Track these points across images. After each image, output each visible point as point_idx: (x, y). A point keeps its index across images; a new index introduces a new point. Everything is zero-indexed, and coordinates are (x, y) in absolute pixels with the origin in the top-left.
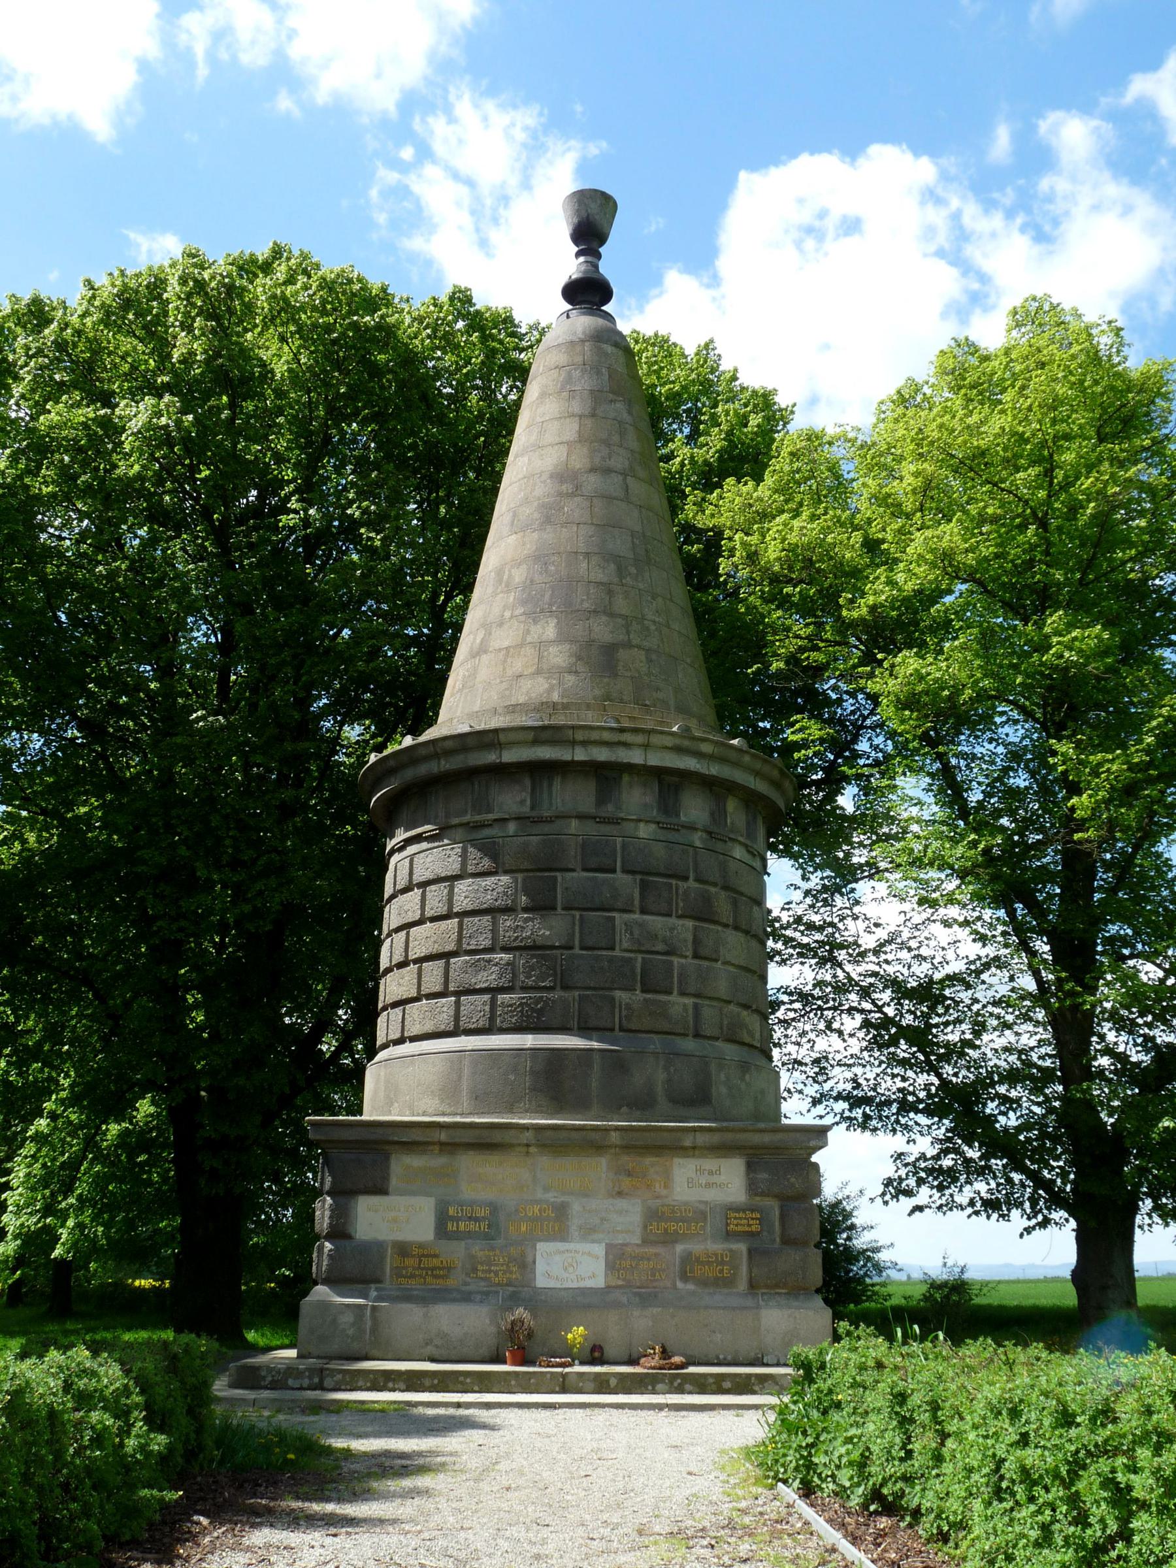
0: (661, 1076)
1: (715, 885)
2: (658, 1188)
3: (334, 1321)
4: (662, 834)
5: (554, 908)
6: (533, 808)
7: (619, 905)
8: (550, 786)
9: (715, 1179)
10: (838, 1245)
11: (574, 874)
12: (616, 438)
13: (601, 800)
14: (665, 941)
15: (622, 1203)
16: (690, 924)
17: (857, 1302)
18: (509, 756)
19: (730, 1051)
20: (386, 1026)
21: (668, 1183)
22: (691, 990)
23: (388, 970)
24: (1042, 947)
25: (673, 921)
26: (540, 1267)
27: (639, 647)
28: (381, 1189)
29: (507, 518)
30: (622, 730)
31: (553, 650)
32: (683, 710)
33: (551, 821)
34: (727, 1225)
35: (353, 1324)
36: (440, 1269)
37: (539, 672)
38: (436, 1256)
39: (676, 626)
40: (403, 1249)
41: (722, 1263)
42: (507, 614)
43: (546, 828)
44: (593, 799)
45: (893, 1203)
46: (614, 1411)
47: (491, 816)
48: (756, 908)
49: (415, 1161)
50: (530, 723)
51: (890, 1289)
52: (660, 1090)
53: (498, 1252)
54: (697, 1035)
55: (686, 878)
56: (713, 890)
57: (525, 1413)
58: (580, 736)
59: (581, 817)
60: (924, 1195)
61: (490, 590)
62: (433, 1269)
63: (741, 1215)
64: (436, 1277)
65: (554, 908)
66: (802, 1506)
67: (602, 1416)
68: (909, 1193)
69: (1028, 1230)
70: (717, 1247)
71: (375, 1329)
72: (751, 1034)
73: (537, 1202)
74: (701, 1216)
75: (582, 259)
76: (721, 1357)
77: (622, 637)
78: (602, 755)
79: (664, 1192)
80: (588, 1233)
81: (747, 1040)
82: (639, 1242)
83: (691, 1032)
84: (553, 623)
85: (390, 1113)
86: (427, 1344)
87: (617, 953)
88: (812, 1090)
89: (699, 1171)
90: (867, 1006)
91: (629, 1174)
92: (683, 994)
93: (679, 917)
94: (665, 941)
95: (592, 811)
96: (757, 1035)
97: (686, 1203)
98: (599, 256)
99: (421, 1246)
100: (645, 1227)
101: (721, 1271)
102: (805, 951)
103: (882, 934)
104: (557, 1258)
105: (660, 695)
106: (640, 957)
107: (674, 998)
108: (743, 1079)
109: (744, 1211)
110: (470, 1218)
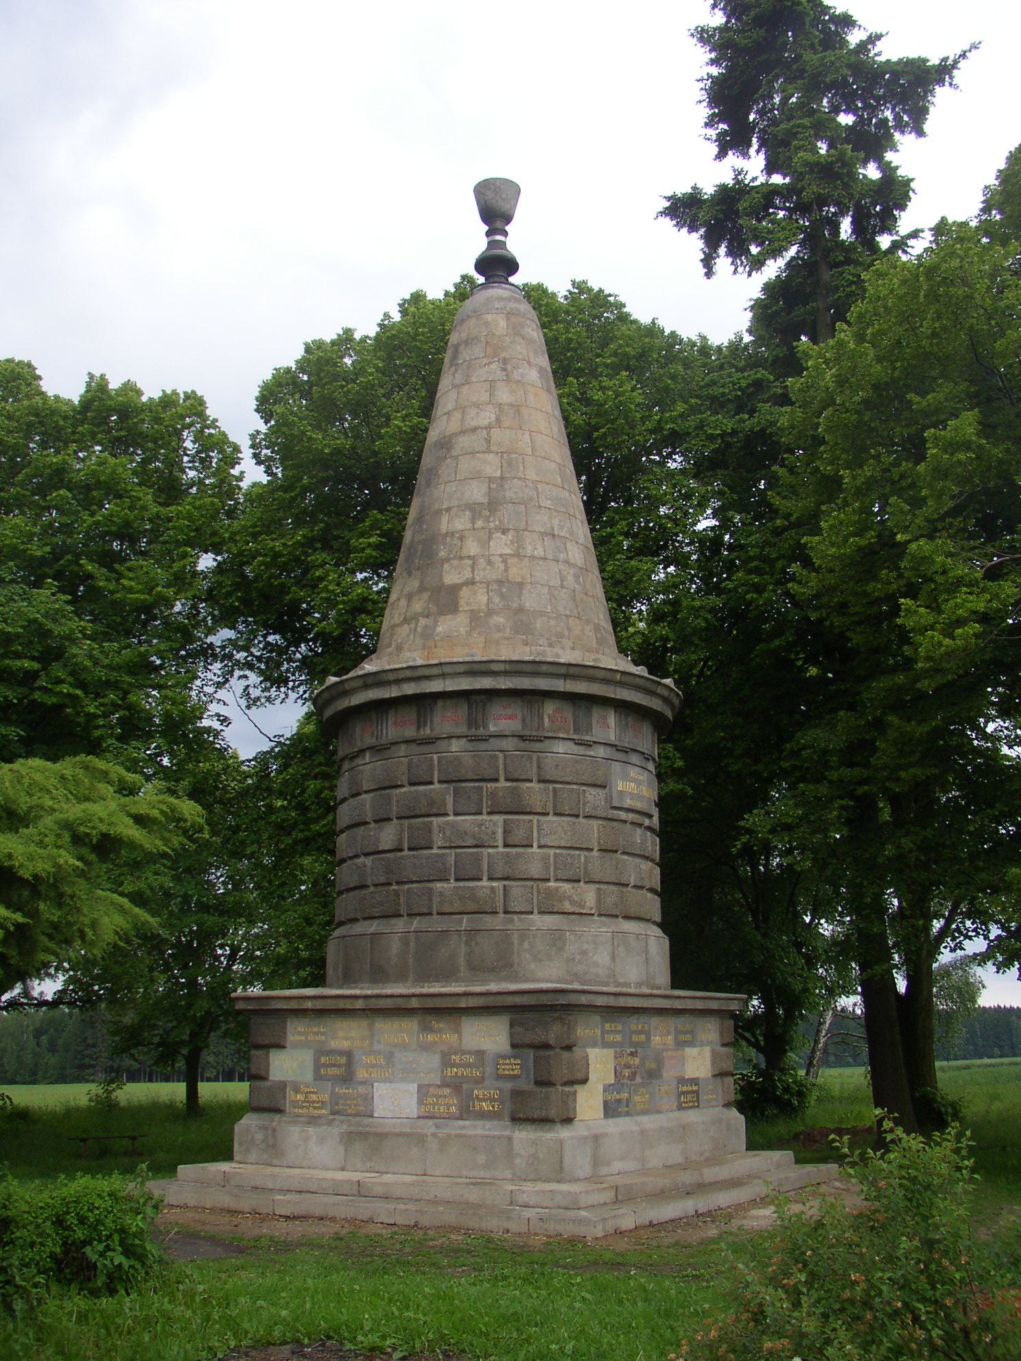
4: (469, 746)
7: (434, 811)
11: (403, 790)
13: (472, 723)
16: (499, 819)
28: (280, 1047)
33: (541, 741)
34: (498, 1069)
36: (318, 1102)
52: (462, 961)
54: (506, 912)
58: (391, 677)
63: (508, 1061)
64: (315, 1108)
83: (500, 908)
87: (435, 851)
92: (491, 879)
93: (489, 813)
106: (453, 852)
107: (485, 883)
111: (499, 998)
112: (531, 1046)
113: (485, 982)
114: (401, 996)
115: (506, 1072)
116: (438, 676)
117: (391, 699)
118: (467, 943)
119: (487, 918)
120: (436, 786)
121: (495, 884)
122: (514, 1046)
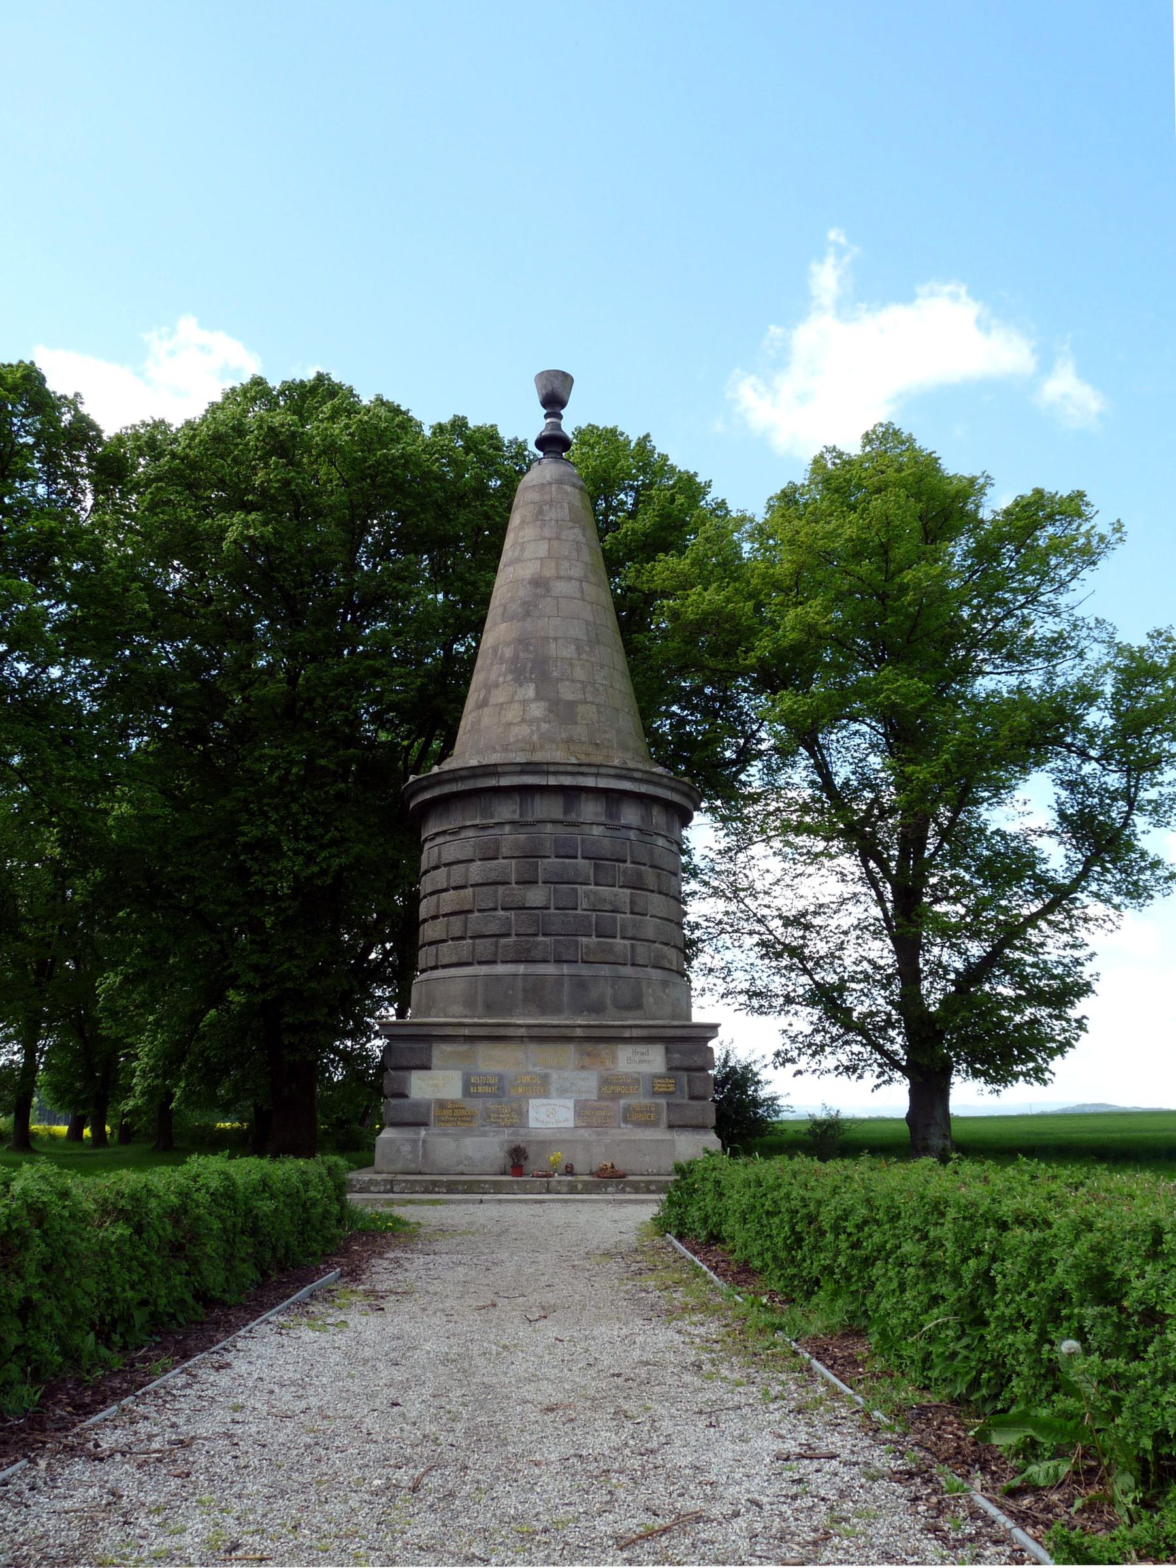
0: (609, 991)
1: (645, 865)
2: (608, 1063)
3: (398, 1150)
5: (536, 882)
6: (521, 815)
7: (580, 880)
8: (533, 801)
9: (645, 1057)
10: (748, 1096)
12: (574, 555)
13: (567, 811)
14: (611, 903)
15: (584, 1074)
16: (628, 891)
17: (762, 1136)
18: (505, 782)
19: (655, 974)
20: (425, 957)
21: (614, 1059)
22: (630, 935)
23: (425, 921)
24: (888, 890)
25: (616, 889)
26: (532, 1114)
27: (592, 703)
29: (500, 611)
30: (580, 765)
31: (533, 706)
32: (624, 747)
37: (523, 720)
39: (618, 686)
40: (442, 1104)
41: (650, 1112)
42: (501, 679)
43: (531, 829)
44: (561, 810)
45: (780, 1068)
46: (580, 1204)
47: (493, 821)
48: (674, 878)
49: (448, 1048)
50: (518, 760)
51: (785, 1126)
52: (608, 1001)
54: (633, 965)
55: (625, 861)
56: (643, 868)
57: (524, 1207)
58: (552, 768)
59: (553, 822)
60: (803, 1062)
61: (488, 661)
62: (462, 1117)
65: (536, 882)
66: (676, 1243)
67: (573, 1207)
68: (792, 1061)
69: (877, 1087)
70: (647, 1101)
71: (425, 1155)
72: (670, 962)
73: (528, 1073)
74: (636, 1081)
75: (549, 420)
77: (580, 696)
78: (567, 781)
79: (612, 1066)
80: (563, 1092)
81: (668, 966)
84: (532, 686)
85: (429, 1016)
87: (579, 912)
88: (721, 989)
89: (636, 1053)
90: (763, 930)
91: (589, 1055)
92: (623, 938)
93: (621, 887)
94: (611, 903)
95: (560, 817)
96: (675, 963)
97: (626, 1074)
98: (560, 417)
99: (453, 1102)
102: (716, 893)
103: (770, 878)
104: (544, 1109)
105: (607, 736)
106: (594, 914)
107: (618, 940)
108: (664, 992)
109: (664, 1078)
110: (485, 1084)
111: (660, 1030)
112: (688, 1069)
113: (626, 1019)
114: (567, 1026)
116: (592, 774)
117: (499, 787)
118: (612, 986)
119: (620, 967)
120: (580, 860)
121: (626, 942)
122: (670, 1069)
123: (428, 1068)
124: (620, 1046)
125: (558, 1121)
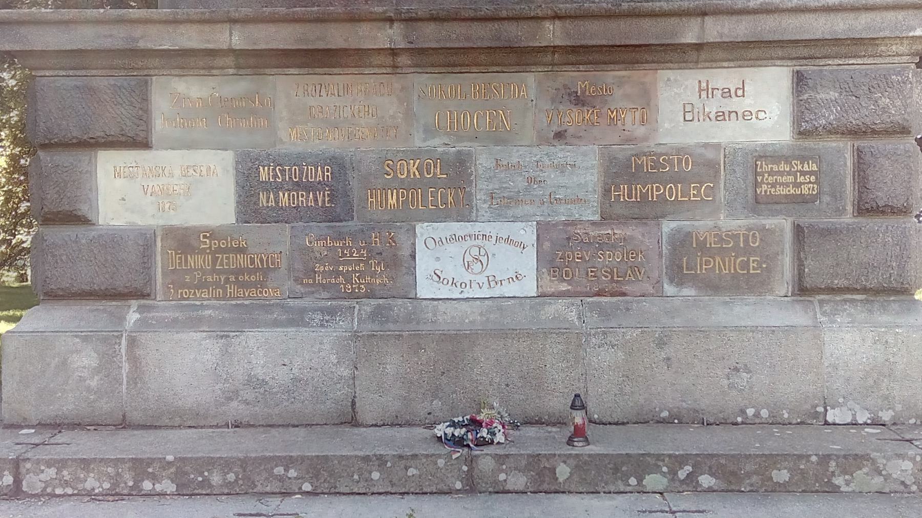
3: (64, 363)
9: (735, 104)
15: (562, 153)
26: (424, 264)
34: (756, 185)
35: (97, 371)
36: (250, 272)
38: (241, 250)
53: (349, 243)
62: (239, 272)
63: (784, 167)
76: (750, 412)
79: (640, 131)
82: (597, 218)
86: (230, 399)
91: (579, 100)
97: (680, 151)
99: (212, 234)
100: (607, 192)
101: (745, 265)
104: (454, 249)
110: (298, 186)
115: (781, 191)
123: (145, 145)
124: (665, 74)
125: (493, 281)
